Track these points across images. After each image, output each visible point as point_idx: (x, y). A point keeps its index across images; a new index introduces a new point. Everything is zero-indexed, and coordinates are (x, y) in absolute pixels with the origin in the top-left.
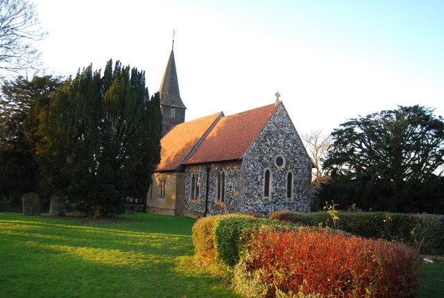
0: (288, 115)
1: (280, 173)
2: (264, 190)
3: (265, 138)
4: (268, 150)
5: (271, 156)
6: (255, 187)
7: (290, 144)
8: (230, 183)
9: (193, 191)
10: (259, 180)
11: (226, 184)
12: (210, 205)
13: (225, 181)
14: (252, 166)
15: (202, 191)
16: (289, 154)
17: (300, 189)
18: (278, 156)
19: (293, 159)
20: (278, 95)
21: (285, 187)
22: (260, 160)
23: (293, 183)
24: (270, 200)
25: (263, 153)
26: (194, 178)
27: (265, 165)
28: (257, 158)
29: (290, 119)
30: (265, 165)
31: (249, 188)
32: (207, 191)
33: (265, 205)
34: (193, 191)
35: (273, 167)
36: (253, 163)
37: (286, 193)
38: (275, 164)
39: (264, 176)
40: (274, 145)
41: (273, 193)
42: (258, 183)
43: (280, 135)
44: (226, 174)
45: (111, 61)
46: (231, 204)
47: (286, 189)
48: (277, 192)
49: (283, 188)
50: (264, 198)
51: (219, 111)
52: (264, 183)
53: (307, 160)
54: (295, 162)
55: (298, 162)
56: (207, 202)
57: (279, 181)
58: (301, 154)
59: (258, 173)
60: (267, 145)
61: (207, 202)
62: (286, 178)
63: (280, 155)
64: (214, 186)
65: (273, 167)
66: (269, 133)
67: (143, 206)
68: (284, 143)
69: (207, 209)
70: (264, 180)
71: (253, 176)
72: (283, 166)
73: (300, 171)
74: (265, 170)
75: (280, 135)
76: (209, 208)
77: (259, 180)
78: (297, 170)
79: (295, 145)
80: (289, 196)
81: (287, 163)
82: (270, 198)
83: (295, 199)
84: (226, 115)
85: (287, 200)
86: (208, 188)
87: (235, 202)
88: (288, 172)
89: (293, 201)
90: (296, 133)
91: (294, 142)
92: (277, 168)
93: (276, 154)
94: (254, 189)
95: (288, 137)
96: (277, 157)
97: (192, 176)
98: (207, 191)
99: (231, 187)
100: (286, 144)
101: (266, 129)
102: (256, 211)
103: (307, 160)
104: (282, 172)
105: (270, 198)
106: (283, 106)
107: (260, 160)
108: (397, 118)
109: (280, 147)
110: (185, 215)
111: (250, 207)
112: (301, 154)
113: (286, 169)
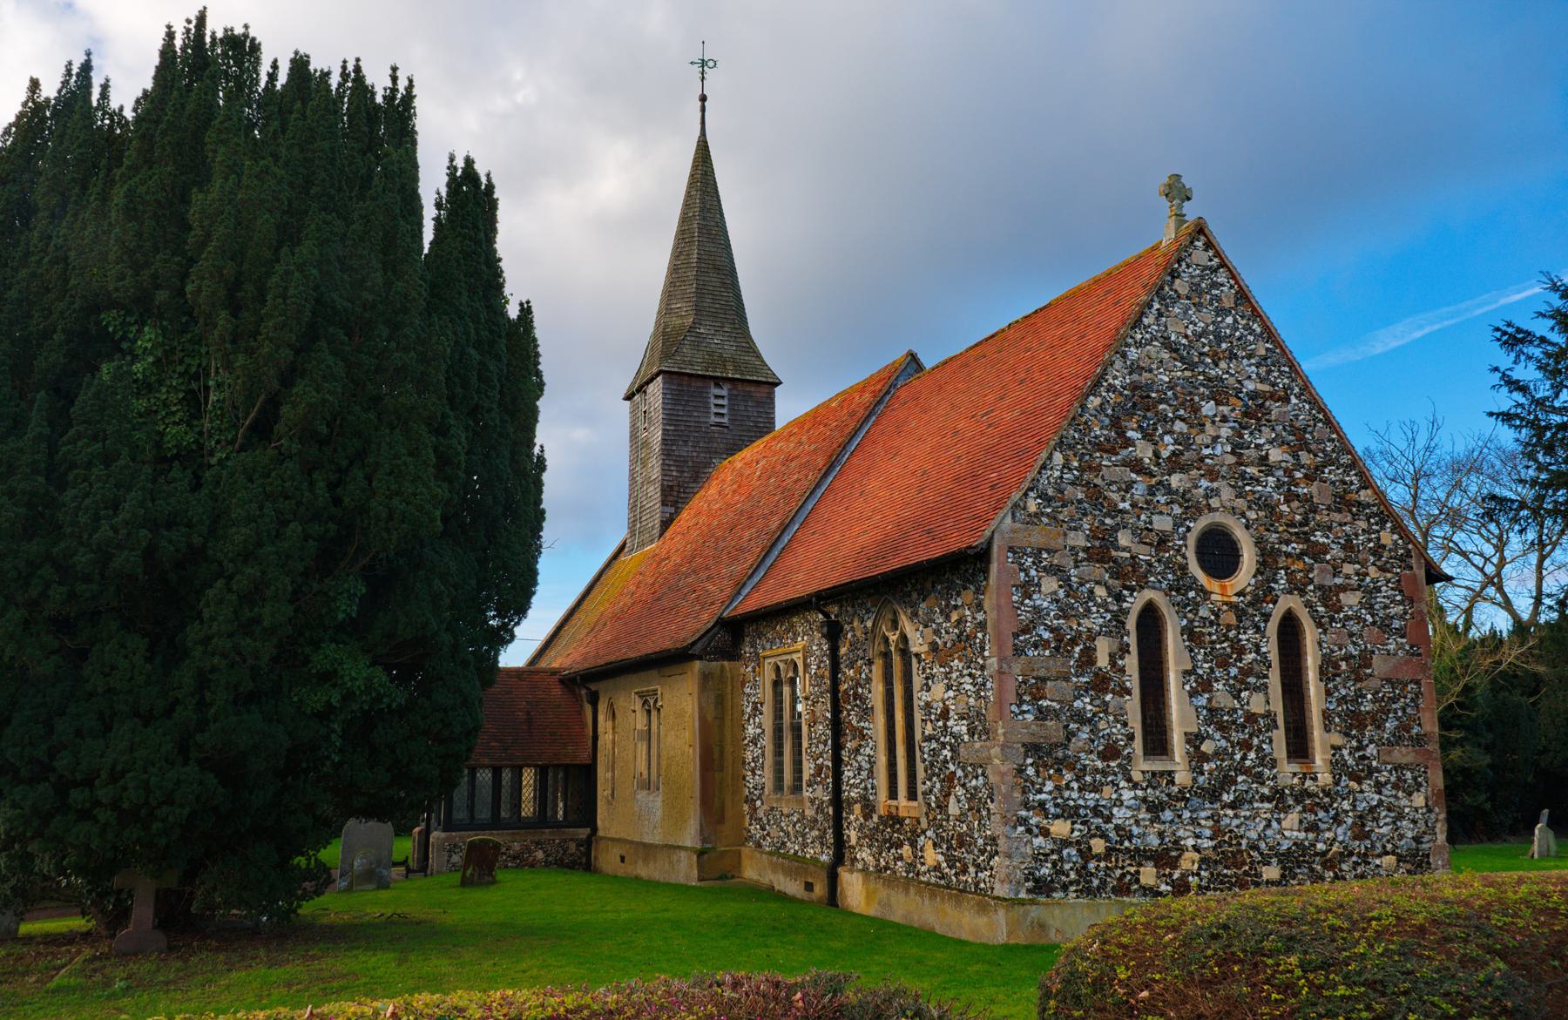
0: (1243, 296)
1: (1230, 618)
2: (1136, 725)
3: (1116, 423)
4: (1139, 491)
5: (1162, 523)
6: (1085, 704)
7: (1276, 455)
8: (938, 690)
9: (778, 752)
10: (1103, 661)
11: (921, 698)
12: (855, 816)
13: (918, 681)
14: (1050, 584)
15: (816, 737)
16: (1269, 507)
17: (1367, 707)
18: (1203, 522)
19: (1305, 538)
20: (1177, 191)
21: (1269, 700)
22: (1101, 549)
23: (1312, 675)
24: (1183, 777)
25: (1114, 511)
26: (777, 684)
27: (1128, 575)
28: (1079, 540)
29: (1256, 314)
30: (1128, 575)
31: (1042, 714)
32: (837, 748)
33: (1155, 808)
34: (778, 752)
35: (1181, 584)
36: (1056, 571)
37: (1279, 735)
38: (1195, 569)
39: (1132, 640)
40: (1176, 464)
41: (1194, 740)
42: (1100, 684)
43: (1208, 408)
44: (918, 644)
45: (70, 63)
46: (953, 809)
47: (1278, 707)
48: (1222, 728)
49: (1257, 704)
50: (1141, 766)
51: (897, 354)
52: (1133, 680)
53: (1387, 538)
54: (1317, 552)
55: (1336, 552)
56: (837, 801)
57: (1224, 664)
58: (1343, 502)
59: (1094, 622)
60: (1137, 466)
61: (837, 801)
62: (1271, 648)
63: (1218, 518)
64: (867, 713)
65: (1181, 584)
66: (1140, 400)
67: (583, 833)
68: (1237, 448)
69: (840, 844)
70: (1131, 662)
71: (1061, 644)
72: (1245, 576)
73: (1350, 600)
74: (1134, 604)
75: (1208, 408)
76: (852, 835)
77: (1103, 661)
78: (1329, 595)
79: (1305, 458)
80: (1299, 748)
81: (1268, 560)
82: (1179, 762)
83: (1338, 767)
84: (928, 362)
85: (1287, 772)
86: (837, 726)
87: (972, 795)
88: (1277, 612)
89: (1325, 778)
90: (1306, 387)
91: (1298, 440)
92: (1205, 593)
93: (1193, 509)
94: (1080, 717)
95: (1255, 412)
96: (1198, 526)
97: (769, 675)
98: (837, 748)
99: (945, 715)
100: (1251, 453)
101: (1118, 377)
102: (1098, 845)
103: (1387, 538)
104: (1240, 613)
105: (1179, 762)
106: (1209, 245)
107: (1101, 549)
108: (1246, 727)
109: (1212, 475)
110: (750, 873)
111: (1060, 828)
112: (1343, 502)
113: (1263, 594)
